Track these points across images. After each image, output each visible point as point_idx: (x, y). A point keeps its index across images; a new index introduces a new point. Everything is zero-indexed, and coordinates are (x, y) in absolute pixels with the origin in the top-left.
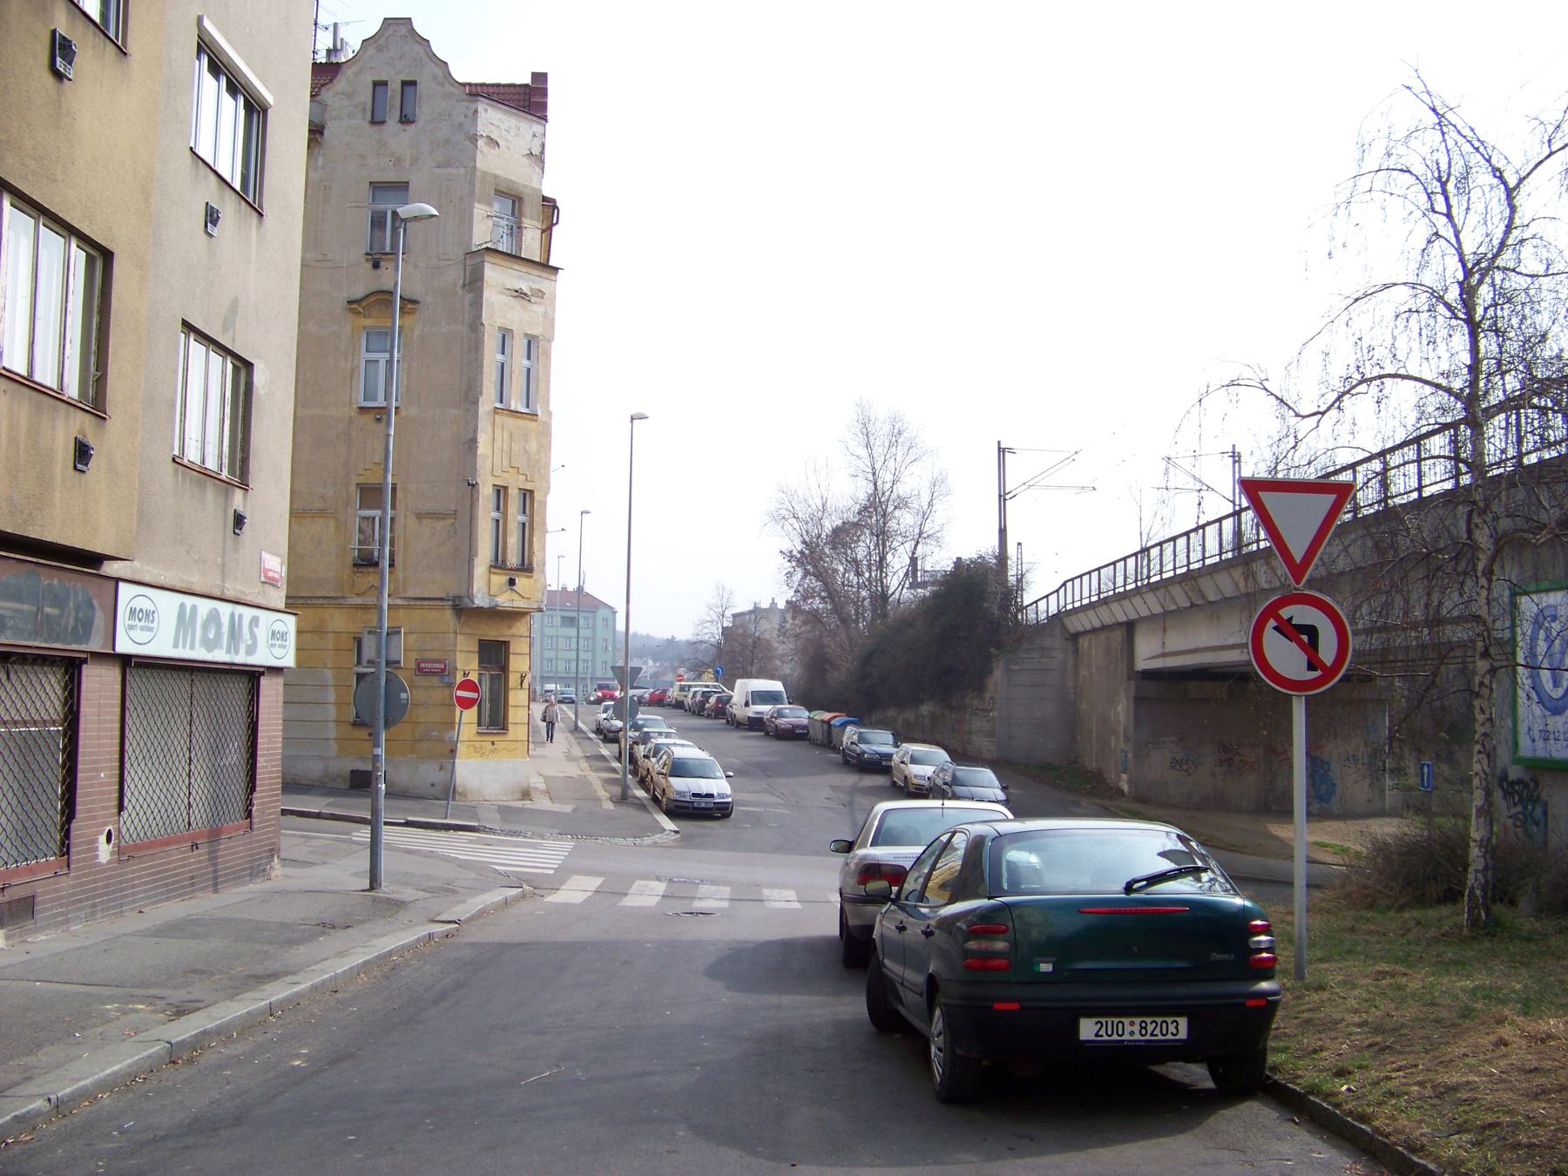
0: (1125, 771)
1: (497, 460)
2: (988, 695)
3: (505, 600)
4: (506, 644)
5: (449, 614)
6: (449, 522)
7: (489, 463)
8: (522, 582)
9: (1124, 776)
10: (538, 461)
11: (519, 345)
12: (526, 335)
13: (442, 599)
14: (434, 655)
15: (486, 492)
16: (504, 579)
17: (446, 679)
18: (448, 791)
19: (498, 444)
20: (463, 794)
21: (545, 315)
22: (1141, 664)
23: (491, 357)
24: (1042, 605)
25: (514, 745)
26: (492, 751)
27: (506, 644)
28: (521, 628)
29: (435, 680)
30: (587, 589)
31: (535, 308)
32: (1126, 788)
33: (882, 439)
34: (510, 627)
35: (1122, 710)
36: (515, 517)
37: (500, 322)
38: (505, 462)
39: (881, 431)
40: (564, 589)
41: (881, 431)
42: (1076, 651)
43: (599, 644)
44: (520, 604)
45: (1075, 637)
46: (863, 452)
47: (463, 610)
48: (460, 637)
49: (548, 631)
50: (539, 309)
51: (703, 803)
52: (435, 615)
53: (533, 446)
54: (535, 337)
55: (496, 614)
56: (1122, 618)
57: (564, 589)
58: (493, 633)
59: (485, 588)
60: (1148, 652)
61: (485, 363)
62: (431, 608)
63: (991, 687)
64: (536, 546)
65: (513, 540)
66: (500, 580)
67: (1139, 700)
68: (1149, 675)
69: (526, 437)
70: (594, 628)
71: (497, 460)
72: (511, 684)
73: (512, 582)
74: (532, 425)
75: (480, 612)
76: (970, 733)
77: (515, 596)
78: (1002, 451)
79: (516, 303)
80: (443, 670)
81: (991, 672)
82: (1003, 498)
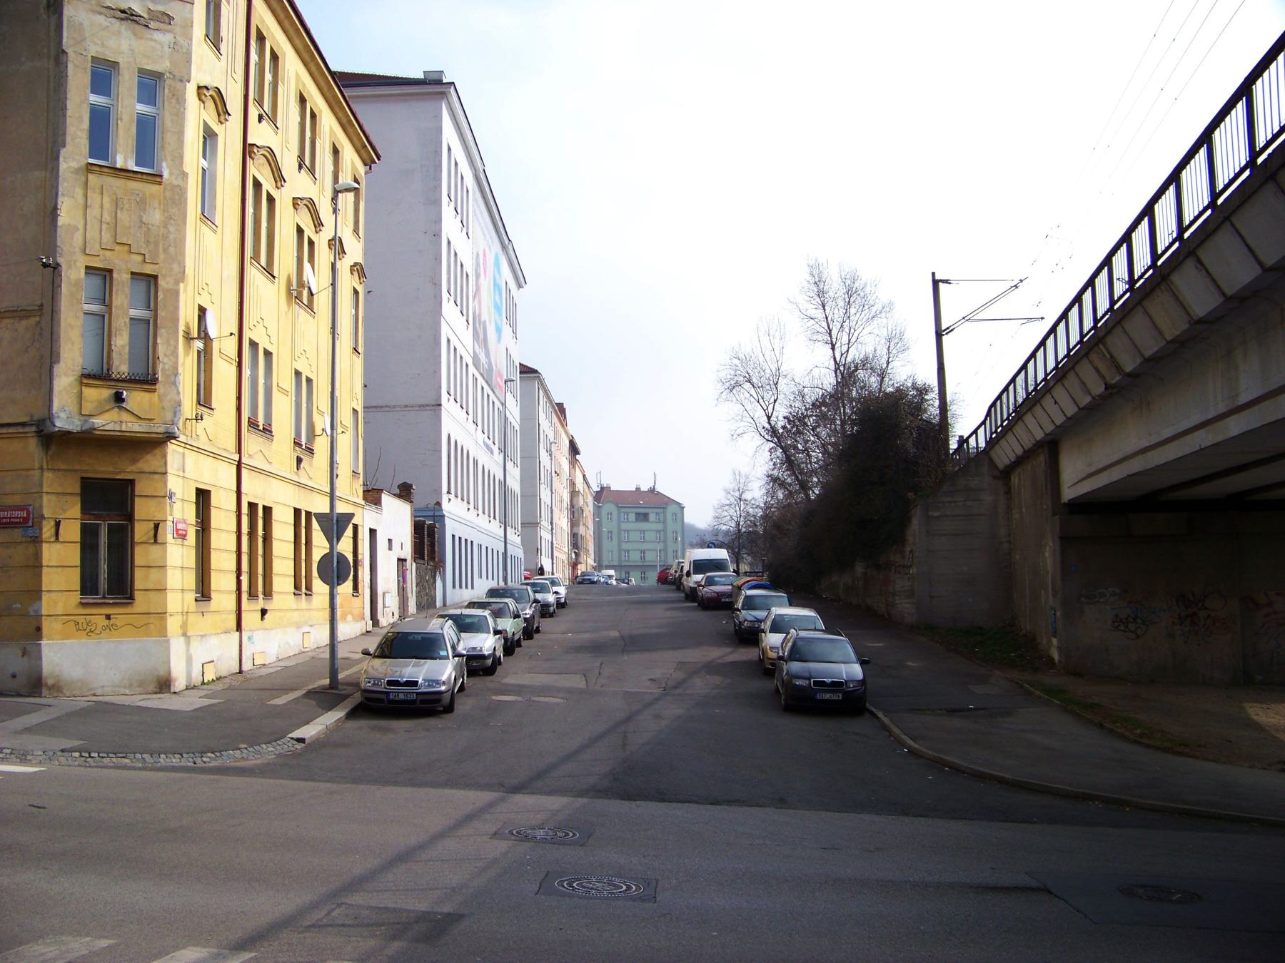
0: (1055, 634)
1: (92, 233)
2: (908, 549)
3: (108, 422)
4: (131, 482)
5: (33, 444)
6: (33, 321)
7: (78, 237)
8: (136, 399)
9: (1055, 641)
10: (165, 237)
11: (127, 84)
12: (142, 72)
13: (24, 424)
14: (16, 500)
15: (73, 272)
16: (106, 393)
17: (30, 532)
18: (35, 685)
19: (94, 212)
20: (57, 688)
21: (175, 46)
22: (1068, 494)
23: (80, 99)
24: (972, 442)
25: (144, 619)
26: (108, 627)
27: (132, 482)
28: (149, 462)
29: (17, 534)
30: (658, 489)
31: (158, 36)
32: (1056, 655)
33: (835, 302)
34: (135, 461)
35: (1049, 556)
36: (126, 307)
37: (94, 50)
38: (107, 237)
39: (835, 288)
40: (638, 489)
41: (835, 288)
42: (1008, 492)
43: (670, 535)
44: (132, 426)
45: (1006, 473)
46: (819, 314)
47: (55, 442)
48: (48, 475)
49: (624, 526)
50: (165, 38)
51: (401, 693)
52: (16, 445)
53: (155, 216)
54: (158, 76)
55: (89, 441)
56: (1039, 435)
57: (638, 489)
58: (104, 468)
59: (70, 403)
60: (1079, 473)
61: (70, 105)
62: (11, 437)
63: (910, 539)
64: (161, 350)
65: (121, 342)
66: (97, 395)
67: (1066, 540)
68: (1080, 506)
69: (142, 204)
70: (664, 522)
71: (92, 233)
72: (137, 538)
73: (118, 398)
74: (154, 189)
75: (66, 438)
76: (894, 594)
77: (125, 416)
78: (936, 283)
79: (124, 28)
80: (26, 520)
81: (909, 520)
82: (939, 335)
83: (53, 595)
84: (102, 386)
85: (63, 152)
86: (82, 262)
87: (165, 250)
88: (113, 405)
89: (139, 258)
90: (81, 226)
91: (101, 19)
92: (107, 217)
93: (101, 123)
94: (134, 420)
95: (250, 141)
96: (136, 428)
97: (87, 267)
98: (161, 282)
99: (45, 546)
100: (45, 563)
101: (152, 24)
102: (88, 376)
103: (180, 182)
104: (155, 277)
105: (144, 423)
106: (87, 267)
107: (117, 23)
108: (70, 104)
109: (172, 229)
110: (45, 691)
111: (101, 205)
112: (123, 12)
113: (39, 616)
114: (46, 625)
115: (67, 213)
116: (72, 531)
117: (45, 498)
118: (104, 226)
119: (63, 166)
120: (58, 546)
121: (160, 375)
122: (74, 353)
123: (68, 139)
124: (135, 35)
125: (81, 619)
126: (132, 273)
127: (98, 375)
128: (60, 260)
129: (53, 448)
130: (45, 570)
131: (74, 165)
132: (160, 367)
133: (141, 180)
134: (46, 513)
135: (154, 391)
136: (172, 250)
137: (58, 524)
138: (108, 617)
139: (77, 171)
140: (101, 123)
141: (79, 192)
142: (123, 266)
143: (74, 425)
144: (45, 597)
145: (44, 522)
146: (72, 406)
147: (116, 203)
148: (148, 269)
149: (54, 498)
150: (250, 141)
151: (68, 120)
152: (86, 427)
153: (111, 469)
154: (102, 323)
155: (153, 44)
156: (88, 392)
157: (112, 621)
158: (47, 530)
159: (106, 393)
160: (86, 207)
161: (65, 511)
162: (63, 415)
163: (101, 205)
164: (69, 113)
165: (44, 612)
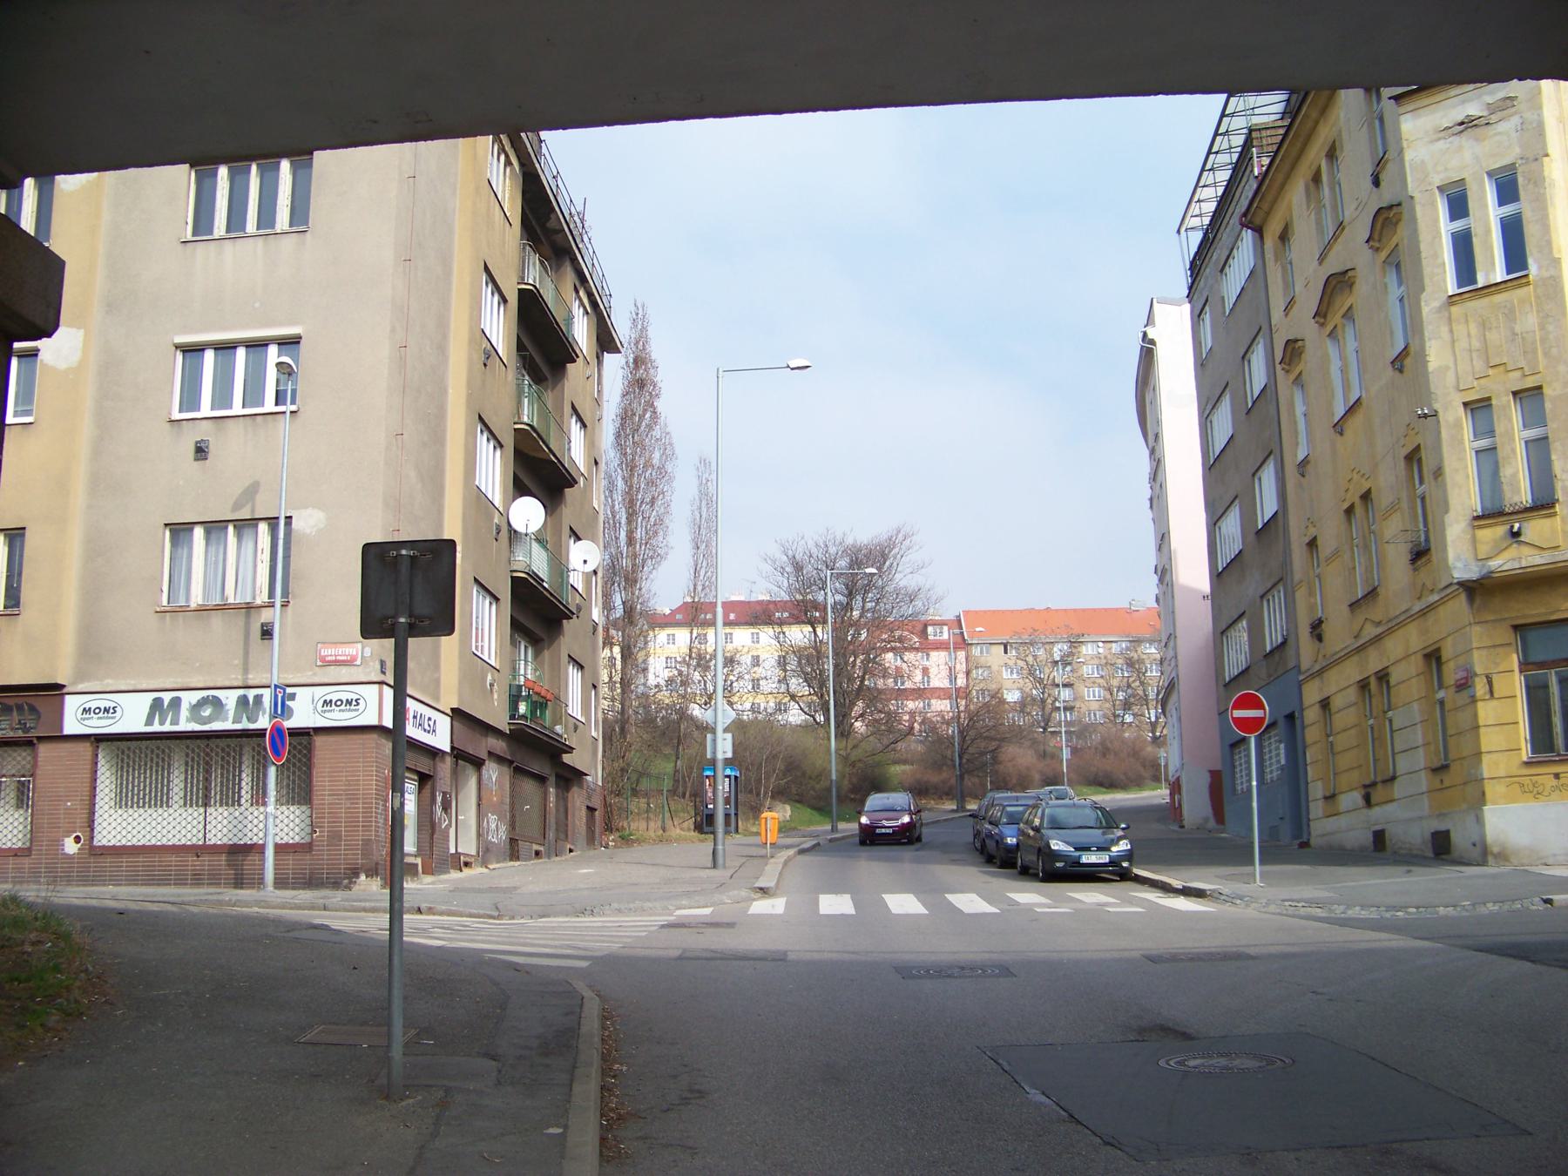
3: (1508, 561)
8: (1535, 529)
15: (1453, 416)
16: (1500, 530)
19: (1462, 344)
20: (1502, 857)
21: (1522, 128)
31: (1502, 127)
38: (1479, 365)
48: (1477, 629)
53: (1529, 321)
66: (1493, 533)
69: (1511, 315)
77: (1526, 550)
83: (1494, 756)
84: (1496, 524)
85: (1424, 296)
86: (1458, 400)
87: (1546, 354)
88: (1510, 541)
89: (1517, 374)
90: (1451, 365)
91: (1441, 145)
92: (1476, 344)
93: (1464, 246)
94: (1536, 552)
95: (319, 741)
96: (1538, 560)
97: (1465, 404)
98: (1546, 391)
99: (1480, 704)
100: (1481, 722)
101: (1494, 118)
102: (1477, 518)
103: (1552, 272)
104: (1540, 387)
105: (1546, 554)
106: (1465, 404)
107: (1456, 139)
108: (1422, 247)
109: (1551, 328)
110: (1490, 859)
111: (1468, 333)
112: (1462, 123)
113: (1480, 780)
114: (1489, 788)
115: (1437, 355)
116: (1515, 684)
117: (1476, 654)
118: (1475, 355)
119: (1425, 310)
120: (1494, 703)
121: (1559, 495)
122: (1463, 492)
123: (1427, 281)
124: (1477, 140)
125: (1526, 780)
126: (1515, 394)
127: (1491, 514)
128: (1436, 406)
129: (1478, 601)
130: (1482, 730)
131: (1436, 304)
132: (1559, 486)
133: (1506, 290)
134: (1478, 669)
135: (1555, 514)
136: (1554, 351)
137: (1490, 683)
138: (1557, 776)
139: (1439, 310)
140: (1464, 246)
141: (1444, 330)
142: (1500, 389)
143: (1472, 573)
144: (1485, 759)
145: (1477, 680)
146: (1467, 554)
147: (1484, 326)
148: (1530, 382)
149: (1484, 652)
150: (319, 741)
151: (1424, 262)
152: (1485, 571)
153: (1543, 610)
154: (1489, 457)
155: (1498, 138)
156: (1481, 533)
157: (1562, 781)
158: (1480, 688)
159: (1500, 530)
160: (1453, 342)
161: (1497, 664)
162: (1459, 565)
163: (1468, 333)
164: (1423, 255)
165: (1486, 775)
